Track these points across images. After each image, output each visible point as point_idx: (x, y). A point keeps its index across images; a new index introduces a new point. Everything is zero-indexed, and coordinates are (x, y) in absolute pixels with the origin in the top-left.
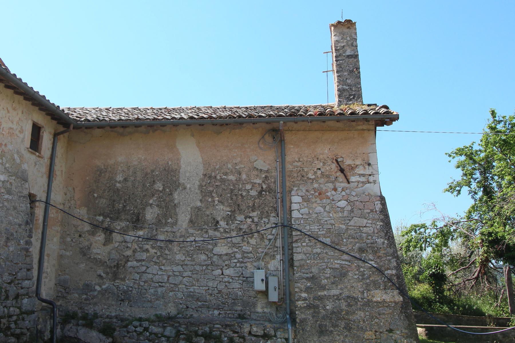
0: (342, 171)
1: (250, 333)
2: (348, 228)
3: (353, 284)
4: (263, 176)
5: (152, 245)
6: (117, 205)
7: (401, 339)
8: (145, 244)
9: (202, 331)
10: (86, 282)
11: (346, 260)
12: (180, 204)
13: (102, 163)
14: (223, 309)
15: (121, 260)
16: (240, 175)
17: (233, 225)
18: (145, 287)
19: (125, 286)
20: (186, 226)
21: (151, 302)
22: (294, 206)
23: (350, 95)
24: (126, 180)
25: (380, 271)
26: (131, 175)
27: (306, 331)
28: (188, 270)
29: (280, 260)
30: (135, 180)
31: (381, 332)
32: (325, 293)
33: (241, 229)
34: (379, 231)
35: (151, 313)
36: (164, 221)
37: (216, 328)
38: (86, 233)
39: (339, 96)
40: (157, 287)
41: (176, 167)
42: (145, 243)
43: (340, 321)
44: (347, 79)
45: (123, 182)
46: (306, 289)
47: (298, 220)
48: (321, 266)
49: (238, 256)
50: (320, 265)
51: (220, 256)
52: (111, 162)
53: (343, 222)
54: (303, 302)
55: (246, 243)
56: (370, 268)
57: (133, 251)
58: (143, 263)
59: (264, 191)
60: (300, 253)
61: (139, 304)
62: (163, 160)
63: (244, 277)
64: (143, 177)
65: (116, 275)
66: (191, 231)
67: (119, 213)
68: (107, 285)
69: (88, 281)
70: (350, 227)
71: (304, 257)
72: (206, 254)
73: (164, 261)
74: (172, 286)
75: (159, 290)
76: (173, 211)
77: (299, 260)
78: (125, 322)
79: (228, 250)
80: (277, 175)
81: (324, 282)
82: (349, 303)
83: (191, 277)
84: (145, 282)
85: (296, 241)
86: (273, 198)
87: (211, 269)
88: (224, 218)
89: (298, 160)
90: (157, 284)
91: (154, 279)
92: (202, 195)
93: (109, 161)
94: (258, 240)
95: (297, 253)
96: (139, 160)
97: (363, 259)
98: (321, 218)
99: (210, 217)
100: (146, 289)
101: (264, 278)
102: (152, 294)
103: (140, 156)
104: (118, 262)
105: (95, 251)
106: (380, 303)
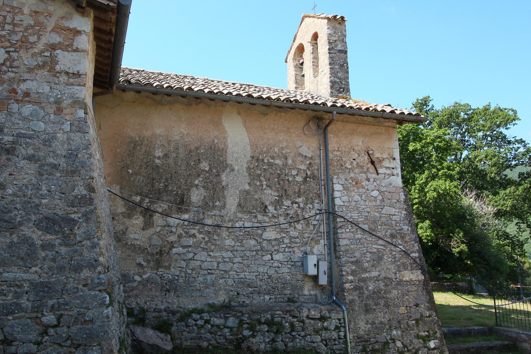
0: (373, 163)
1: (308, 317)
2: (381, 216)
3: (388, 266)
4: (308, 162)
5: (199, 230)
6: (157, 184)
7: (425, 312)
8: (191, 229)
9: (264, 318)
10: (123, 272)
11: (381, 245)
12: (228, 186)
13: (136, 134)
14: (273, 293)
15: (165, 246)
16: (286, 160)
17: (281, 210)
18: (194, 275)
19: (169, 275)
20: (235, 210)
21: (200, 290)
22: (337, 194)
23: (340, 88)
24: (166, 156)
25: (406, 253)
26: (172, 151)
27: (355, 311)
28: (238, 256)
29: (325, 245)
30: (177, 157)
31: (410, 307)
32: (367, 275)
33: (288, 214)
34: (404, 219)
35: (199, 304)
36: (211, 204)
37: (277, 315)
38: (121, 215)
39: (332, 87)
40: (206, 274)
41: (223, 146)
42: (192, 227)
43: (380, 300)
44: (338, 72)
45: (163, 157)
46: (352, 272)
47: (341, 207)
48: (362, 251)
49: (287, 241)
50: (361, 249)
51: (269, 241)
52: (147, 133)
53: (376, 210)
54: (350, 284)
55: (292, 229)
56: (400, 252)
57: (179, 237)
58: (190, 249)
59: (308, 177)
60: (345, 238)
61: (187, 294)
62: (209, 137)
63: (292, 262)
64: (186, 155)
65: (159, 263)
66: (239, 215)
67: (160, 194)
68: (148, 274)
69: (124, 271)
70: (382, 215)
71: (348, 242)
72: (255, 239)
73: (213, 247)
74: (222, 272)
75: (209, 277)
76: (221, 194)
77: (344, 246)
78: (186, 316)
79: (276, 235)
80: (320, 163)
81: (366, 265)
82: (386, 283)
83: (242, 263)
84: (192, 270)
85: (341, 227)
86: (316, 185)
87: (261, 254)
88: (272, 203)
89: (337, 150)
90: (206, 272)
91: (203, 267)
92: (250, 178)
93: (144, 132)
94: (304, 226)
95: (342, 239)
96: (181, 135)
97: (394, 244)
98: (359, 206)
99: (258, 202)
100: (194, 278)
101: (316, 264)
102: (201, 282)
103: (182, 130)
104: (161, 248)
105: (132, 236)
106: (408, 281)
